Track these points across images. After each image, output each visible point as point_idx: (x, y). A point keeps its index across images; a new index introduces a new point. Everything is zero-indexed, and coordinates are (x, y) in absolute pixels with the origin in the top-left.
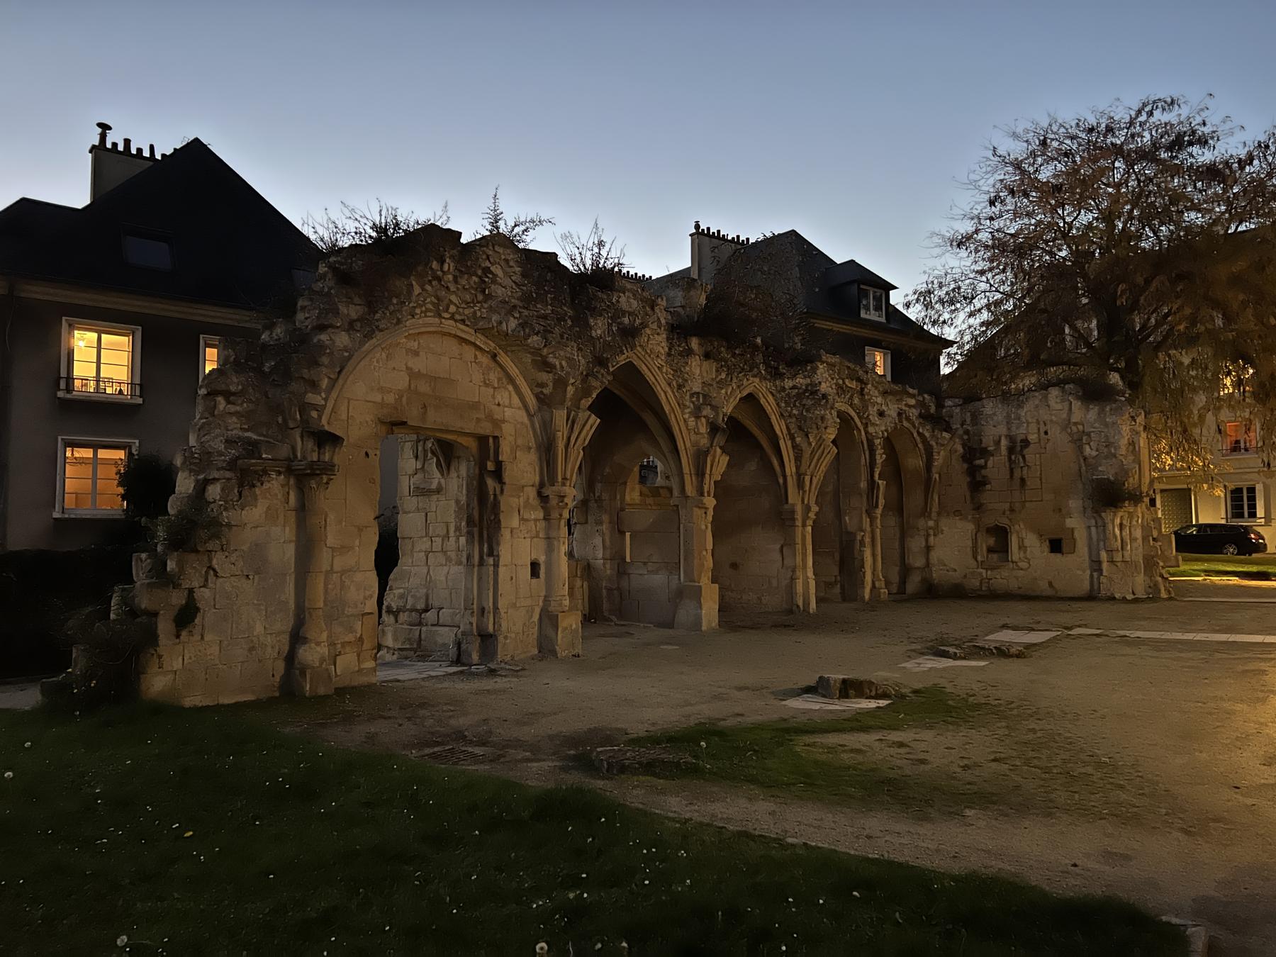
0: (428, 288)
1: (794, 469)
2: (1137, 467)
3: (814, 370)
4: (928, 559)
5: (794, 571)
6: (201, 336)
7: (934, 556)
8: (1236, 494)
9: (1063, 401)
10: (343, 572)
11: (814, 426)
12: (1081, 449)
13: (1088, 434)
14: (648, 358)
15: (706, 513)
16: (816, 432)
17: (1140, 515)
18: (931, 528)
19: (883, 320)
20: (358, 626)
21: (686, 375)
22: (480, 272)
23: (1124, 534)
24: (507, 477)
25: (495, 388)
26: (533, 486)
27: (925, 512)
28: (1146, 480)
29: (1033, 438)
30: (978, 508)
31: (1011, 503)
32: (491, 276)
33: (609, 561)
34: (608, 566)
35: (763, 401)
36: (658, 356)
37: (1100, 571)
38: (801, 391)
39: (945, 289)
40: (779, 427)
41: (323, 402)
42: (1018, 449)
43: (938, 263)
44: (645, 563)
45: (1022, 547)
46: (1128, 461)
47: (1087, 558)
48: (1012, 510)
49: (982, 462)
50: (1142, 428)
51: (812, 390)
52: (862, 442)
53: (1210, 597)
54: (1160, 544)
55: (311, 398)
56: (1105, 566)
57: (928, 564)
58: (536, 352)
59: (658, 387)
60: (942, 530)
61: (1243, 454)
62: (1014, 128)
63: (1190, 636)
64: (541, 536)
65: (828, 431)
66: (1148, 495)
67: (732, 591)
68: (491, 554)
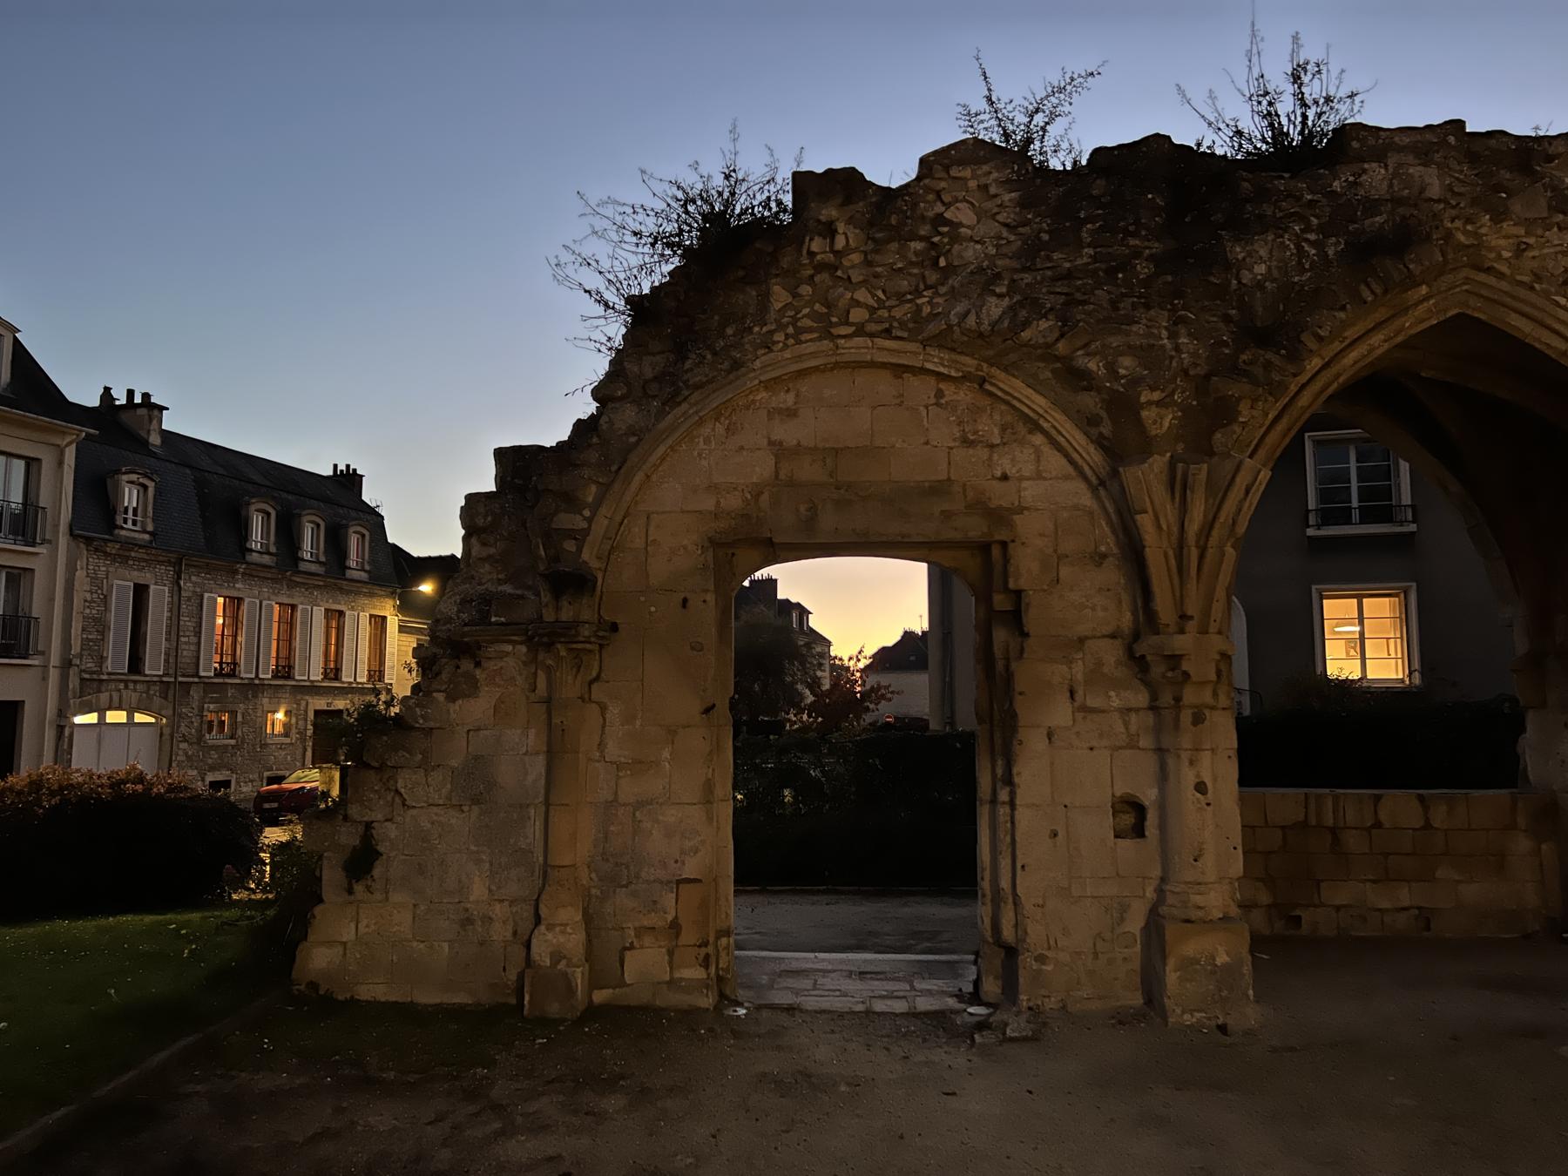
0: (806, 290)
6: (1307, 435)
10: (640, 804)
14: (1532, 297)
20: (669, 900)
22: (924, 230)
24: (1031, 620)
25: (992, 446)
26: (1113, 636)
32: (946, 229)
41: (585, 525)
55: (565, 520)
58: (1046, 353)
64: (1142, 744)
68: (1009, 781)
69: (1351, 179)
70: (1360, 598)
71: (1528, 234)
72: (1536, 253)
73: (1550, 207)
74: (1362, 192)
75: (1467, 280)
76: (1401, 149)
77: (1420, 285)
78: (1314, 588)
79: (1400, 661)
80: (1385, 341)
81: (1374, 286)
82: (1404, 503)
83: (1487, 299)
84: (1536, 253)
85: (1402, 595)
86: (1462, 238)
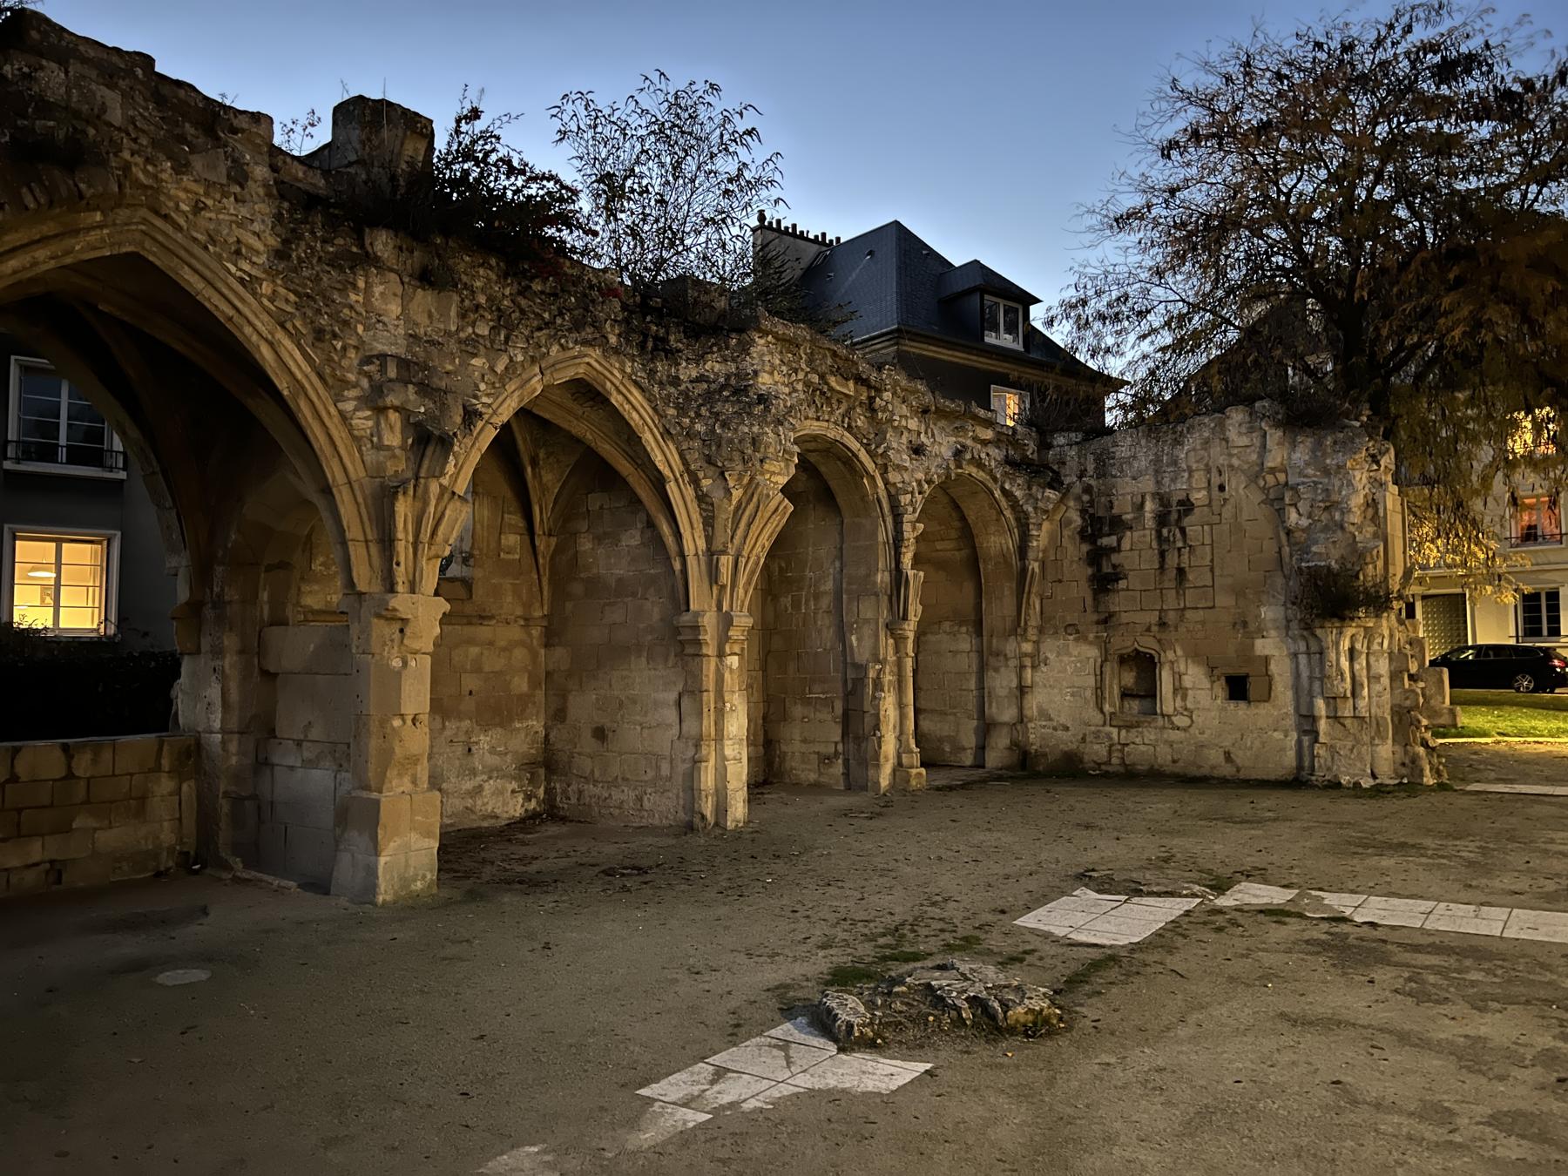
1: (702, 544)
2: (1381, 549)
3: (745, 348)
4: (1021, 709)
5: (697, 746)
7: (1033, 703)
8: (1530, 604)
9: (1251, 430)
11: (736, 456)
12: (1280, 513)
13: (1294, 488)
15: (402, 631)
16: (740, 467)
17: (1386, 633)
18: (1026, 655)
19: (1019, 347)
21: (346, 311)
23: (1357, 667)
27: (1017, 628)
28: (1398, 570)
29: (1199, 496)
30: (1106, 621)
31: (1161, 611)
33: (236, 736)
34: (233, 747)
35: (616, 399)
36: (238, 253)
37: (1314, 734)
38: (713, 386)
39: (1105, 299)
40: (664, 457)
42: (1174, 516)
43: (1093, 256)
44: (299, 743)
45: (1179, 690)
46: (1365, 535)
47: (1291, 710)
48: (1162, 624)
49: (1111, 541)
50: (1389, 478)
51: (739, 388)
52: (879, 500)
53: (1512, 781)
54: (1422, 685)
56: (1323, 725)
57: (1021, 719)
59: (248, 330)
60: (1047, 658)
61: (1540, 544)
62: (1205, 54)
63: (1492, 922)
65: (766, 466)
66: (1400, 597)
67: (595, 782)
69: (26, 70)
70: (59, 542)
71: (207, 194)
72: (213, 215)
73: (229, 176)
74: (36, 88)
75: (145, 221)
76: (85, 61)
77: (95, 210)
78: (6, 527)
79: (97, 611)
80: (53, 258)
81: (37, 192)
82: (115, 449)
83: (162, 245)
84: (213, 215)
85: (105, 543)
86: (141, 176)
